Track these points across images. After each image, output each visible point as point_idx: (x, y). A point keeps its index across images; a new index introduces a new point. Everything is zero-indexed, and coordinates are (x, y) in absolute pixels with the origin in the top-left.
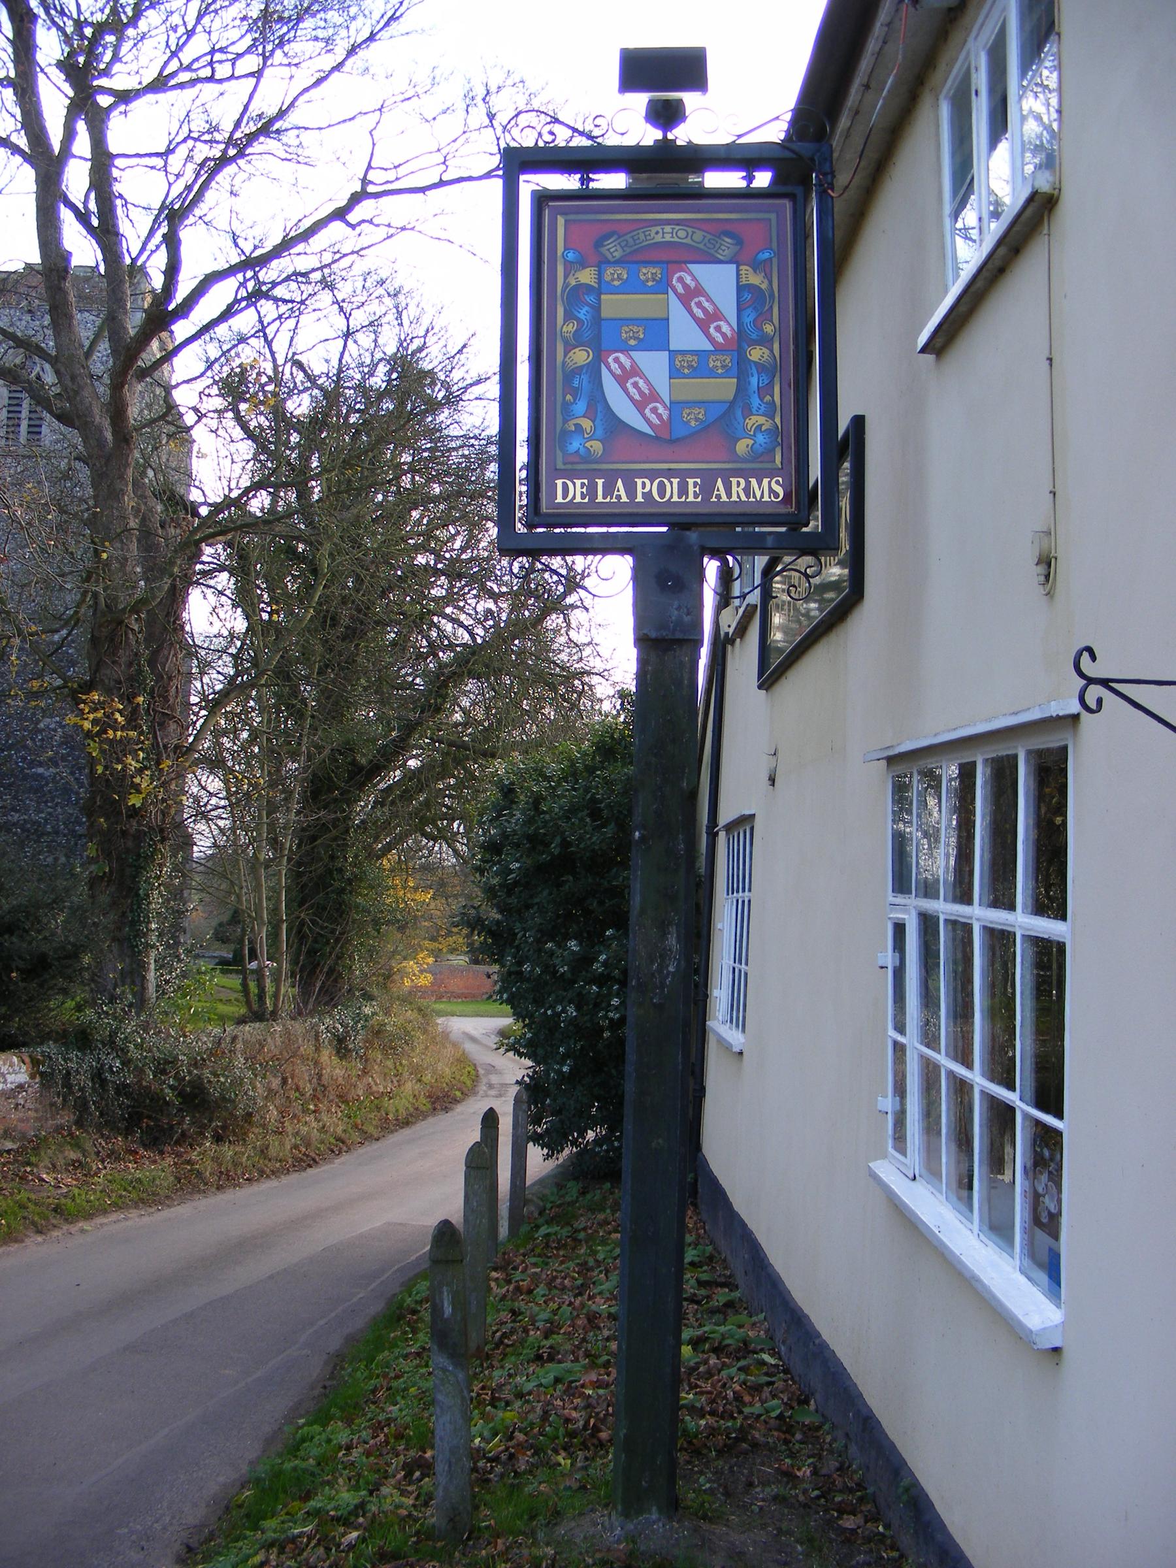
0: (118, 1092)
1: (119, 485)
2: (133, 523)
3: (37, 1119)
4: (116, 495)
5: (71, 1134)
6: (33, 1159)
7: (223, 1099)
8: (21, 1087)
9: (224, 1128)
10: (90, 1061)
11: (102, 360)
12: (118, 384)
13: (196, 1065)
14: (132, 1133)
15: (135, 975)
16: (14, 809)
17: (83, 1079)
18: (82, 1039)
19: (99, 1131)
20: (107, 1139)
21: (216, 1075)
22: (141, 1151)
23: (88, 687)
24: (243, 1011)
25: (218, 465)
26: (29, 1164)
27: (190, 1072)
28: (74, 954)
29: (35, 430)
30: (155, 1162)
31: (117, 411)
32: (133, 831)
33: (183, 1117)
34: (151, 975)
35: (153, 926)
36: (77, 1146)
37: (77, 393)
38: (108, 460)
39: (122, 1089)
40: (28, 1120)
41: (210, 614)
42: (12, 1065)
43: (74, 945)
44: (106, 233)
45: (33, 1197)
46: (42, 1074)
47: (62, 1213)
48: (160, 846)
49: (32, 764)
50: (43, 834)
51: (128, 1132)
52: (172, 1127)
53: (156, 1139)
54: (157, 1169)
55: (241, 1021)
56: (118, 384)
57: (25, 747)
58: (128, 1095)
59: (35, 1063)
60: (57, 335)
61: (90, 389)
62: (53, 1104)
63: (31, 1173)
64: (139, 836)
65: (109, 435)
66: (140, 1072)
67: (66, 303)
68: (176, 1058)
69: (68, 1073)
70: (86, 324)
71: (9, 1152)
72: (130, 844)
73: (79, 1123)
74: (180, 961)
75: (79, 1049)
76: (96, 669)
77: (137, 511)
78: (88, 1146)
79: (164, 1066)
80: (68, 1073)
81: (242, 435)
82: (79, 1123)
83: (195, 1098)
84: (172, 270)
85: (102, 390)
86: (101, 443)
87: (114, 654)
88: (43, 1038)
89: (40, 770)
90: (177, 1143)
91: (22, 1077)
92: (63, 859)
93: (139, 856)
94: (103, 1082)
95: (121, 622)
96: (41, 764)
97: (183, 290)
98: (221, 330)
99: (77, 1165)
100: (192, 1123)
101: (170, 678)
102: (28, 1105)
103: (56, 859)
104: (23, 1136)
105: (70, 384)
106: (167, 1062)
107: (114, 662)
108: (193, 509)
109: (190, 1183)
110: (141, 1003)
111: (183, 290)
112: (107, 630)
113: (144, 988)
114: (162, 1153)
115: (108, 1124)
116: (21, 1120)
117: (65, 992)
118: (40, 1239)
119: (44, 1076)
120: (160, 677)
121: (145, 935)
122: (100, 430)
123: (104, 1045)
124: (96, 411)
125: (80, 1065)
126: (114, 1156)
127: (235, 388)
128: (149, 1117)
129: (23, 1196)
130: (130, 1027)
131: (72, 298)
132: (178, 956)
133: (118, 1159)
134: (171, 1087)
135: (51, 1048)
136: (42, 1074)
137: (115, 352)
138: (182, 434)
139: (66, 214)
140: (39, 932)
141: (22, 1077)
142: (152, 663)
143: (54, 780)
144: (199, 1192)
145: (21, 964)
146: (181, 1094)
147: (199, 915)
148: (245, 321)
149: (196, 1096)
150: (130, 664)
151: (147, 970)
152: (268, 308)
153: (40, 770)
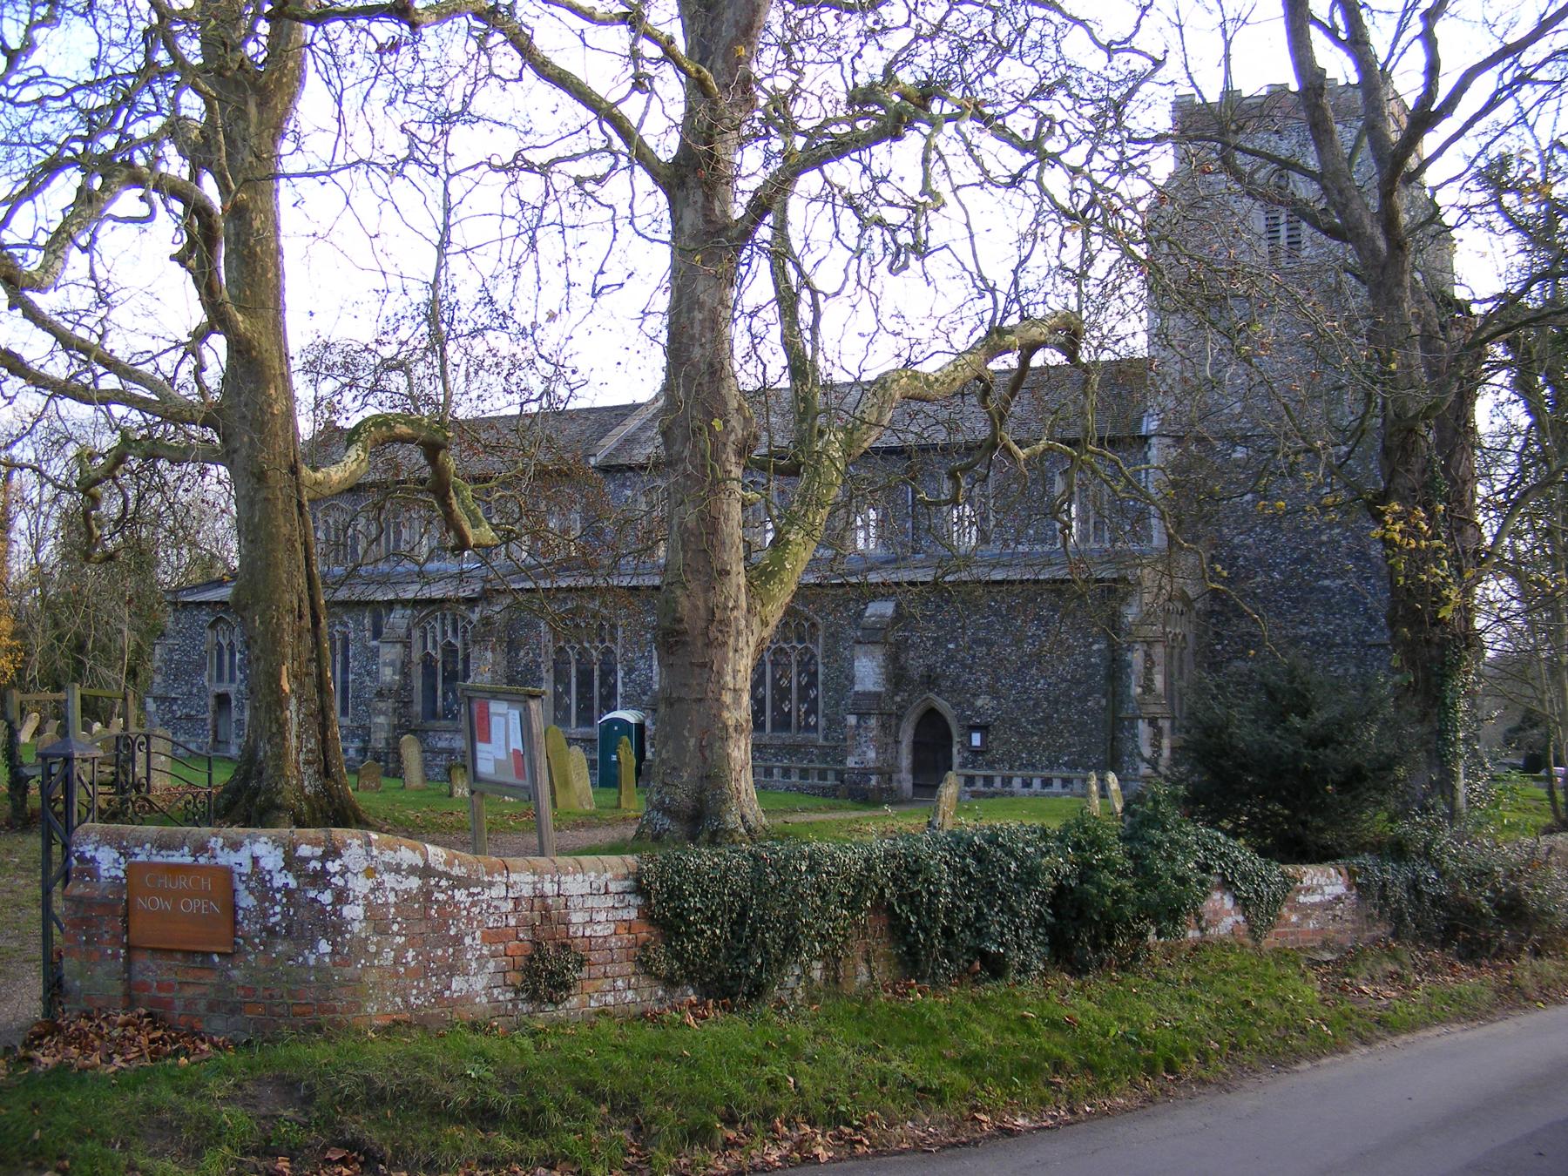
0: (1433, 903)
1: (1397, 292)
2: (1416, 329)
3: (1354, 931)
4: (1396, 303)
5: (1388, 946)
6: (1352, 971)
7: (1543, 912)
8: (1338, 898)
9: (1542, 942)
10: (1406, 872)
11: (1365, 171)
12: (1387, 193)
13: (1511, 876)
14: (1449, 945)
15: (1446, 785)
16: (1302, 622)
17: (1399, 891)
18: (1397, 850)
19: (1415, 943)
20: (1423, 951)
21: (1534, 888)
22: (1459, 964)
23: (1384, 497)
24: (1548, 820)
25: (1484, 265)
26: (1347, 975)
27: (1506, 884)
28: (1388, 764)
29: (1294, 243)
30: (1473, 975)
31: (1388, 218)
32: (1436, 639)
33: (1501, 931)
34: (1461, 784)
35: (1461, 735)
36: (1394, 957)
37: (1346, 206)
38: (1384, 268)
39: (1437, 901)
40: (1344, 931)
41: (1496, 411)
42: (1329, 877)
43: (1388, 757)
44: (1356, 44)
45: (1356, 1008)
46: (1358, 886)
47: (1387, 1025)
48: (1465, 653)
49: (1319, 576)
50: (1333, 645)
51: (1443, 945)
52: (1489, 940)
53: (1474, 953)
54: (1473, 982)
55: (1549, 831)
56: (1387, 193)
57: (1310, 560)
58: (1444, 907)
59: (1352, 874)
60: (1320, 150)
61: (1358, 201)
62: (1370, 916)
63: (1351, 984)
64: (1443, 645)
65: (1382, 244)
66: (1455, 883)
67: (1326, 119)
68: (1492, 870)
69: (1384, 885)
70: (1345, 135)
71: (1327, 963)
72: (1434, 652)
73: (1395, 935)
74: (1485, 769)
75: (1394, 861)
76: (1391, 477)
77: (1417, 317)
78: (1405, 958)
79: (1482, 875)
80: (1384, 885)
81: (1506, 226)
82: (1395, 935)
83: (1513, 910)
84: (1432, 70)
85: (1374, 203)
86: (1375, 252)
87: (1407, 463)
88: (1359, 849)
89: (1327, 582)
90: (1495, 956)
91: (1340, 889)
92: (1353, 671)
93: (1444, 664)
94: (1419, 894)
95: (1411, 431)
96: (1327, 577)
97: (1445, 87)
98: (1480, 126)
99: (1396, 977)
100: (1511, 936)
101: (1465, 482)
102: (1346, 917)
103: (1347, 670)
104: (1341, 948)
105: (1338, 198)
106: (1482, 873)
107: (1407, 471)
108: (1463, 307)
109: (1513, 997)
110: (1453, 815)
111: (1445, 87)
112: (1399, 441)
113: (1454, 799)
114: (1479, 966)
115: (1425, 937)
116: (1338, 932)
117: (1379, 803)
118: (1365, 1050)
119: (1361, 888)
120: (1454, 482)
121: (1453, 744)
122: (1372, 239)
123: (1419, 856)
124: (1367, 221)
125: (1394, 875)
126: (1430, 968)
127: (1495, 177)
128: (1466, 930)
129: (1345, 1007)
130: (1445, 837)
131: (1330, 113)
132: (1483, 765)
133: (1435, 972)
134: (1487, 899)
135: (1366, 859)
136: (1358, 886)
137: (1379, 160)
138: (1443, 235)
139: (1315, 34)
140: (1352, 744)
141: (1340, 889)
142: (1445, 469)
143: (1341, 592)
144: (1520, 1007)
145: (1336, 777)
146: (1497, 906)
147: (1495, 716)
148: (1505, 112)
149: (1513, 909)
150: (1424, 471)
151: (1456, 779)
152: (1527, 94)
153: (1327, 582)
